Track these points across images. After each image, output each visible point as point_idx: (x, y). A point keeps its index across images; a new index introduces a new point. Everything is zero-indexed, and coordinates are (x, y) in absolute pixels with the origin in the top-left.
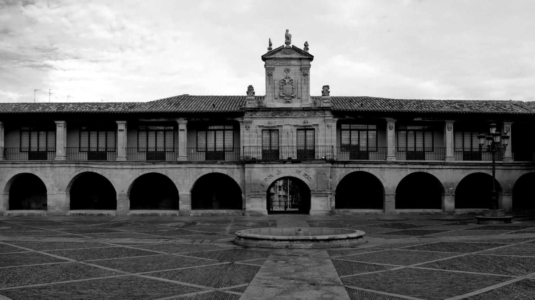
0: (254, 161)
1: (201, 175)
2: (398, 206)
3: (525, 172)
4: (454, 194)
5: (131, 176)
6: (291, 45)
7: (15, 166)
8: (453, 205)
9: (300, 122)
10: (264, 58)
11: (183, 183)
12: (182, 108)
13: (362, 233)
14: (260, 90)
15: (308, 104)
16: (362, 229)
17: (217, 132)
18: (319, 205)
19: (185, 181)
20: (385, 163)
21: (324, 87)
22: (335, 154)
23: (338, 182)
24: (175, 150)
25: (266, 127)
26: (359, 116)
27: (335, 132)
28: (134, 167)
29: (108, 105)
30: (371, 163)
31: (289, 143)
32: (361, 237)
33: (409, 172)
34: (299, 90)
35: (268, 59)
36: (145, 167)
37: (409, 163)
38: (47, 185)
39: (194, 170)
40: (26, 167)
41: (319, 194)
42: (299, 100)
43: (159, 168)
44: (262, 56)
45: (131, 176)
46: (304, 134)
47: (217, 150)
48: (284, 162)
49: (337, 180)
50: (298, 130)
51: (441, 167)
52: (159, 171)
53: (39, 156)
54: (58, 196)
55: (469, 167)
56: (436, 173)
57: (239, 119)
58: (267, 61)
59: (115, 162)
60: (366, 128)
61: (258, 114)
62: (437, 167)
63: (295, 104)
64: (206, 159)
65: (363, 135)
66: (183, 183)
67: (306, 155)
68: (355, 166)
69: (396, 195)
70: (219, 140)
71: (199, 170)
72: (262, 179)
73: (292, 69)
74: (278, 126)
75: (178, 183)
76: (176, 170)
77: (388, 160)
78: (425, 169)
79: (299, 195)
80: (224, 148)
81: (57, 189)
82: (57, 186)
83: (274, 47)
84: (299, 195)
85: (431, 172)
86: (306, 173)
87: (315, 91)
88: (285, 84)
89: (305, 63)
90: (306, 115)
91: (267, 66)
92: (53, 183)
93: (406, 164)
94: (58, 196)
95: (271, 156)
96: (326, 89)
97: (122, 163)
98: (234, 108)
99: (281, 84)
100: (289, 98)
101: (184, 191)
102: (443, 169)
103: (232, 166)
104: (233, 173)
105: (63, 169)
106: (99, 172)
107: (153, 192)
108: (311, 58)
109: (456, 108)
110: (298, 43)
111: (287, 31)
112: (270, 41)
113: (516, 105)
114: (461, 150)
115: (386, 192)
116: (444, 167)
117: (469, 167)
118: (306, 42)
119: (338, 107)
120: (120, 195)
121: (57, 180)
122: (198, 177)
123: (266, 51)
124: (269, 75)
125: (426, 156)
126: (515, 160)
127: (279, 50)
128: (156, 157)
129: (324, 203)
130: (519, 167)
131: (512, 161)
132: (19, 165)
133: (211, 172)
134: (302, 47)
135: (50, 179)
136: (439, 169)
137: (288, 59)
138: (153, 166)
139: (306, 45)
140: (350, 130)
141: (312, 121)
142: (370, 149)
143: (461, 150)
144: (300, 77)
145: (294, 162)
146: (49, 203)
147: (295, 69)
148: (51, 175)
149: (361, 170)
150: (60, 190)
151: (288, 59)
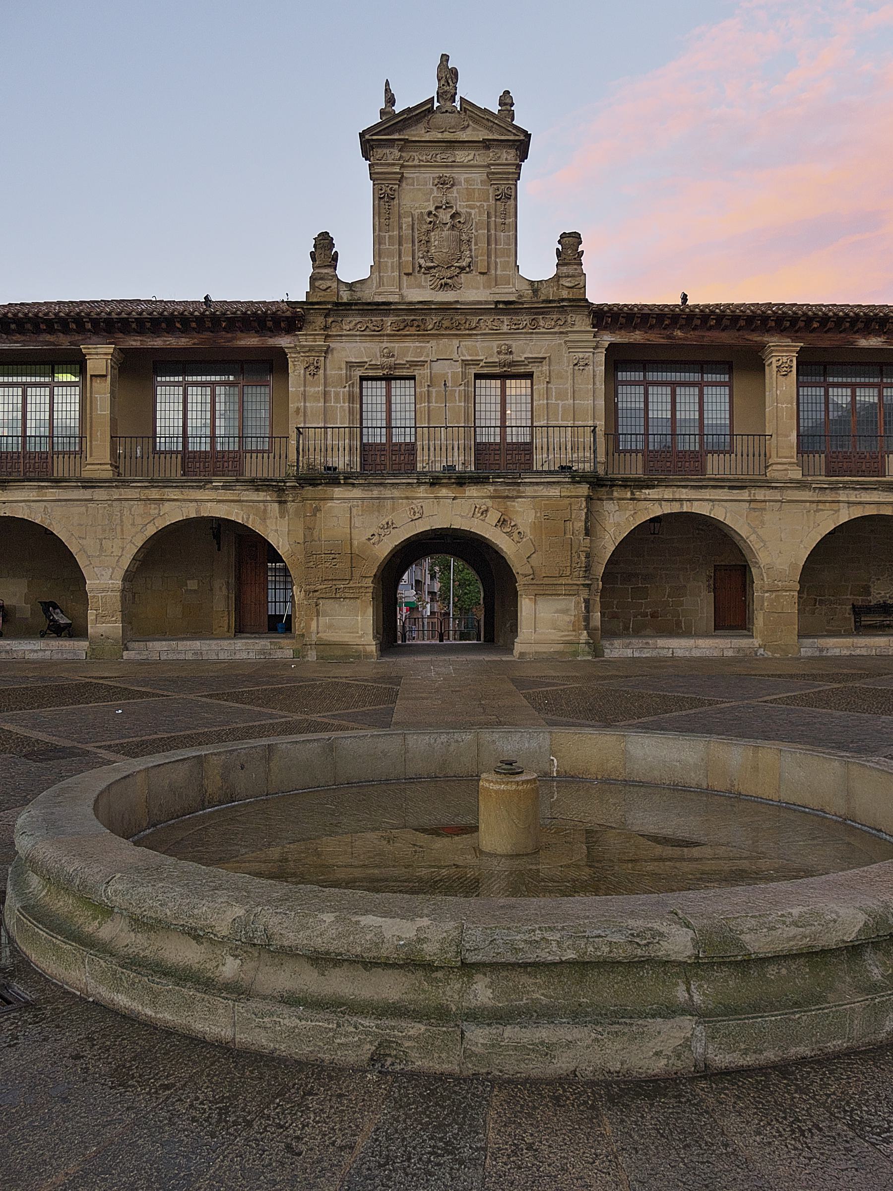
0: (332, 477)
1: (161, 524)
9: (484, 349)
18: (545, 623)
20: (768, 484)
21: (564, 236)
22: (601, 458)
25: (374, 367)
27: (601, 387)
33: (845, 516)
35: (382, 144)
39: (138, 508)
41: (546, 589)
42: (481, 278)
44: (362, 135)
46: (500, 851)
47: (248, 455)
48: (435, 482)
57: (284, 341)
58: (379, 152)
61: (351, 322)
63: (473, 292)
68: (668, 494)
71: (153, 510)
74: (413, 364)
75: (83, 550)
76: (62, 506)
79: (487, 580)
87: (536, 263)
90: (505, 329)
91: (378, 169)
95: (385, 464)
96: (570, 248)
100: (450, 272)
103: (262, 496)
104: (264, 520)
110: (479, 91)
111: (445, 58)
112: (387, 90)
118: (507, 92)
122: (151, 530)
124: (385, 199)
127: (421, 113)
129: (565, 619)
134: (495, 108)
139: (506, 100)
140: (647, 384)
141: (525, 348)
145: (462, 481)
147: (467, 180)
151: (443, 149)
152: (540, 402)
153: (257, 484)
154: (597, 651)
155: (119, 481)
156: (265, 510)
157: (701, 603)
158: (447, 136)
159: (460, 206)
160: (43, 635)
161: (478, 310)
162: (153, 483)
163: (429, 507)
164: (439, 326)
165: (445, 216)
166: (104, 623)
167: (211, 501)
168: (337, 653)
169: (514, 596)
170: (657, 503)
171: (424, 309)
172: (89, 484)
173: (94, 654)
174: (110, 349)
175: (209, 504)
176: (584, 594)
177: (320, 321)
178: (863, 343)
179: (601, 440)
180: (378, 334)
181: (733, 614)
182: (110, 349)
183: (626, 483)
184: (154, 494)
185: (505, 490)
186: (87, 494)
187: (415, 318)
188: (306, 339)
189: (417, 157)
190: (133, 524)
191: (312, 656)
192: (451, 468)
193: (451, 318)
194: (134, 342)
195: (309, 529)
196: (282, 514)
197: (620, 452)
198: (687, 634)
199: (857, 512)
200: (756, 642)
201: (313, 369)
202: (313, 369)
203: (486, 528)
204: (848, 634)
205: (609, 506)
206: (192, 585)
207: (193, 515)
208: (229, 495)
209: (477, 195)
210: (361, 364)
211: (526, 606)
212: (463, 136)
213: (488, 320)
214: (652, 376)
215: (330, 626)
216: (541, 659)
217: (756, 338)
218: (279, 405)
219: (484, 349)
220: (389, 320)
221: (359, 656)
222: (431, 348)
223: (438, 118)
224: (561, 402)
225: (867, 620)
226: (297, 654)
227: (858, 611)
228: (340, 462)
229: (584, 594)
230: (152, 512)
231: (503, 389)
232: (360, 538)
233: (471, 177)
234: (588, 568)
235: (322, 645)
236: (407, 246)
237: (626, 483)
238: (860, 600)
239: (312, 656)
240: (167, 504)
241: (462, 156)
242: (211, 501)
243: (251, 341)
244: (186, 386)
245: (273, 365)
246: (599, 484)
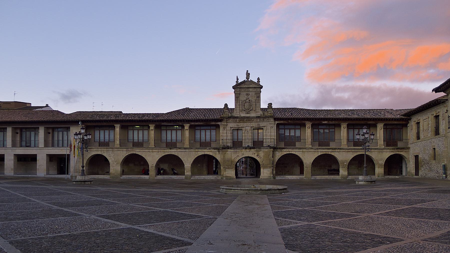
6: (249, 80)
8: (346, 173)
9: (254, 125)
10: (234, 87)
12: (186, 117)
14: (232, 105)
15: (260, 113)
17: (207, 131)
20: (305, 148)
24: (182, 141)
26: (289, 120)
29: (144, 115)
30: (296, 148)
31: (247, 136)
33: (320, 154)
36: (166, 151)
37: (320, 149)
38: (110, 161)
39: (194, 153)
41: (265, 167)
43: (173, 152)
45: (157, 156)
48: (246, 148)
50: (278, 125)
51: (339, 151)
53: (105, 144)
54: (115, 167)
55: (356, 151)
56: (336, 154)
57: (219, 123)
59: (148, 148)
62: (337, 151)
63: (253, 115)
67: (257, 144)
68: (287, 150)
70: (205, 135)
76: (183, 153)
77: (307, 146)
78: (329, 152)
79: (254, 167)
82: (115, 162)
83: (240, 81)
84: (254, 167)
85: (333, 154)
86: (260, 156)
87: (264, 105)
89: (258, 90)
93: (317, 149)
94: (115, 167)
95: (237, 144)
96: (270, 105)
97: (152, 149)
98: (217, 117)
103: (215, 151)
106: (139, 154)
108: (262, 87)
109: (349, 115)
110: (253, 78)
111: (247, 71)
113: (388, 112)
116: (341, 151)
117: (356, 151)
119: (279, 115)
121: (115, 158)
122: (196, 157)
123: (235, 84)
124: (237, 98)
125: (331, 144)
127: (244, 82)
128: (171, 145)
131: (383, 147)
132: (94, 150)
137: (247, 89)
138: (170, 151)
139: (258, 79)
141: (262, 124)
145: (251, 148)
146: (111, 171)
149: (291, 153)
151: (247, 89)
152: (264, 134)
153: (215, 149)
154: (274, 178)
155: (190, 148)
157: (298, 170)
158: (248, 86)
159: (250, 99)
160: (172, 175)
161: (253, 118)
162: (197, 148)
164: (247, 120)
165: (248, 101)
166: (188, 173)
168: (228, 178)
170: (285, 152)
171: (244, 117)
172: (185, 149)
173: (186, 178)
174: (189, 125)
176: (272, 168)
177: (226, 120)
178: (323, 122)
179: (275, 140)
180: (236, 122)
181: (302, 172)
182: (189, 125)
183: (280, 148)
184: (197, 150)
185: (258, 150)
186: (185, 150)
187: (242, 119)
188: (223, 123)
189: (243, 90)
191: (224, 178)
192: (248, 146)
193: (249, 119)
194: (193, 123)
195: (224, 156)
196: (219, 154)
198: (295, 175)
199: (322, 153)
200: (304, 176)
201: (224, 128)
202: (224, 128)
203: (255, 156)
204: (327, 175)
205: (277, 152)
206: (199, 165)
208: (210, 150)
211: (262, 170)
212: (251, 86)
213: (255, 119)
215: (228, 173)
216: (264, 179)
217: (304, 122)
218: (218, 133)
219: (254, 125)
220: (238, 119)
221: (233, 179)
222: (245, 124)
223: (246, 83)
224: (269, 133)
226: (221, 178)
227: (328, 170)
228: (229, 145)
229: (272, 168)
232: (233, 158)
233: (252, 93)
234: (273, 163)
235: (226, 177)
236: (241, 106)
237: (280, 148)
238: (329, 168)
239: (224, 178)
241: (251, 90)
243: (214, 123)
244: (200, 130)
245: (218, 127)
246: (275, 149)
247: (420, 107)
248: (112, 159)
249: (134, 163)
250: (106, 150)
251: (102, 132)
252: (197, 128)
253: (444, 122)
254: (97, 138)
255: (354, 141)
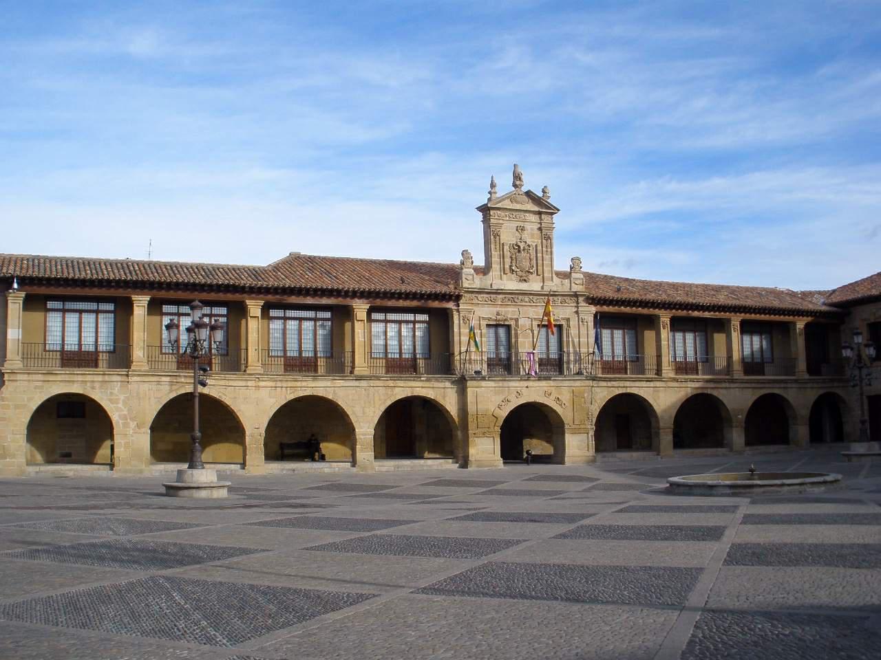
2: (271, 456)
3: (821, 392)
4: (743, 425)
5: (273, 400)
7: (51, 378)
11: (364, 413)
13: (839, 477)
16: (838, 472)
19: (367, 410)
23: (599, 410)
28: (279, 384)
32: (836, 481)
34: (540, 262)
36: (299, 384)
38: (115, 417)
39: (382, 390)
40: (73, 382)
41: (576, 432)
45: (273, 400)
49: (595, 409)
51: (727, 385)
52: (321, 393)
60: (413, 319)
62: (723, 385)
63: (534, 285)
64: (177, 369)
65: (405, 330)
66: (364, 413)
67: (554, 366)
68: (621, 384)
69: (673, 429)
72: (492, 407)
73: (528, 226)
75: (354, 413)
80: (763, 360)
81: (133, 425)
85: (715, 393)
88: (519, 251)
92: (126, 412)
95: (505, 365)
99: (512, 250)
101: (365, 428)
102: (730, 388)
104: (444, 397)
105: (146, 386)
107: (305, 429)
114: (280, 354)
115: (661, 424)
116: (732, 385)
120: (252, 435)
121: (132, 403)
122: (389, 403)
126: (676, 374)
130: (815, 385)
131: (807, 376)
132: (59, 378)
133: (624, 392)
134: (540, 195)
135: (120, 405)
136: (726, 388)
140: (285, 319)
142: (765, 360)
143: (280, 354)
144: (540, 241)
148: (122, 397)
149: (629, 391)
150: (138, 426)
156: (444, 392)
163: (524, 391)
167: (419, 387)
169: (563, 434)
175: (418, 389)
180: (493, 303)
190: (380, 400)
197: (47, 351)
207: (410, 395)
208: (427, 384)
209: (535, 236)
210: (517, 325)
211: (567, 436)
214: (69, 305)
225: (287, 451)
230: (389, 393)
231: (80, 319)
240: (397, 389)
242: (419, 387)
247: (405, 264)
248: (118, 409)
249: (192, 426)
250: (100, 378)
251: (72, 319)
252: (50, 305)
253: (524, 391)
254: (54, 339)
255: (62, 351)
